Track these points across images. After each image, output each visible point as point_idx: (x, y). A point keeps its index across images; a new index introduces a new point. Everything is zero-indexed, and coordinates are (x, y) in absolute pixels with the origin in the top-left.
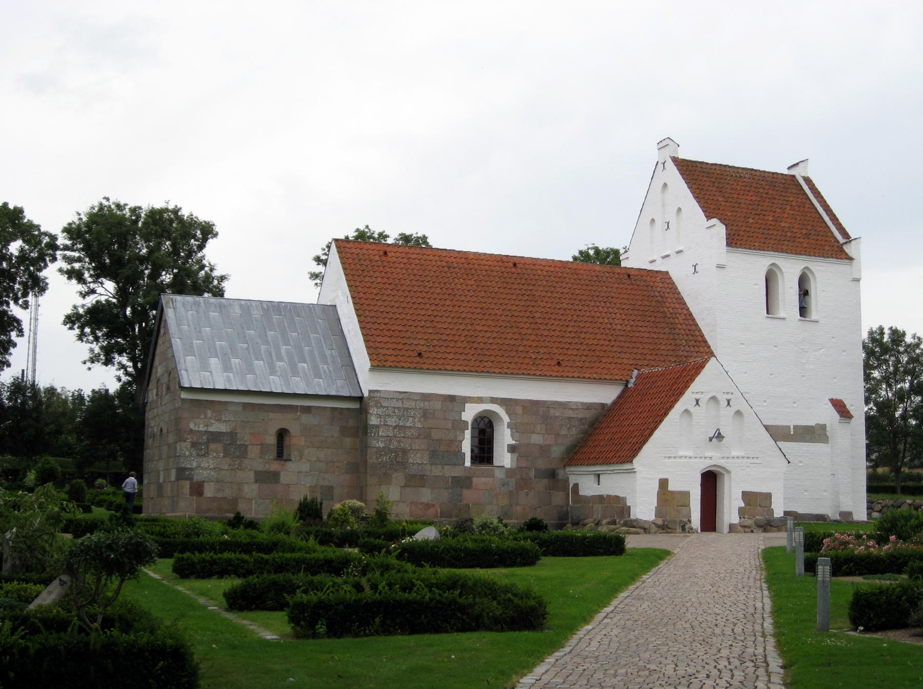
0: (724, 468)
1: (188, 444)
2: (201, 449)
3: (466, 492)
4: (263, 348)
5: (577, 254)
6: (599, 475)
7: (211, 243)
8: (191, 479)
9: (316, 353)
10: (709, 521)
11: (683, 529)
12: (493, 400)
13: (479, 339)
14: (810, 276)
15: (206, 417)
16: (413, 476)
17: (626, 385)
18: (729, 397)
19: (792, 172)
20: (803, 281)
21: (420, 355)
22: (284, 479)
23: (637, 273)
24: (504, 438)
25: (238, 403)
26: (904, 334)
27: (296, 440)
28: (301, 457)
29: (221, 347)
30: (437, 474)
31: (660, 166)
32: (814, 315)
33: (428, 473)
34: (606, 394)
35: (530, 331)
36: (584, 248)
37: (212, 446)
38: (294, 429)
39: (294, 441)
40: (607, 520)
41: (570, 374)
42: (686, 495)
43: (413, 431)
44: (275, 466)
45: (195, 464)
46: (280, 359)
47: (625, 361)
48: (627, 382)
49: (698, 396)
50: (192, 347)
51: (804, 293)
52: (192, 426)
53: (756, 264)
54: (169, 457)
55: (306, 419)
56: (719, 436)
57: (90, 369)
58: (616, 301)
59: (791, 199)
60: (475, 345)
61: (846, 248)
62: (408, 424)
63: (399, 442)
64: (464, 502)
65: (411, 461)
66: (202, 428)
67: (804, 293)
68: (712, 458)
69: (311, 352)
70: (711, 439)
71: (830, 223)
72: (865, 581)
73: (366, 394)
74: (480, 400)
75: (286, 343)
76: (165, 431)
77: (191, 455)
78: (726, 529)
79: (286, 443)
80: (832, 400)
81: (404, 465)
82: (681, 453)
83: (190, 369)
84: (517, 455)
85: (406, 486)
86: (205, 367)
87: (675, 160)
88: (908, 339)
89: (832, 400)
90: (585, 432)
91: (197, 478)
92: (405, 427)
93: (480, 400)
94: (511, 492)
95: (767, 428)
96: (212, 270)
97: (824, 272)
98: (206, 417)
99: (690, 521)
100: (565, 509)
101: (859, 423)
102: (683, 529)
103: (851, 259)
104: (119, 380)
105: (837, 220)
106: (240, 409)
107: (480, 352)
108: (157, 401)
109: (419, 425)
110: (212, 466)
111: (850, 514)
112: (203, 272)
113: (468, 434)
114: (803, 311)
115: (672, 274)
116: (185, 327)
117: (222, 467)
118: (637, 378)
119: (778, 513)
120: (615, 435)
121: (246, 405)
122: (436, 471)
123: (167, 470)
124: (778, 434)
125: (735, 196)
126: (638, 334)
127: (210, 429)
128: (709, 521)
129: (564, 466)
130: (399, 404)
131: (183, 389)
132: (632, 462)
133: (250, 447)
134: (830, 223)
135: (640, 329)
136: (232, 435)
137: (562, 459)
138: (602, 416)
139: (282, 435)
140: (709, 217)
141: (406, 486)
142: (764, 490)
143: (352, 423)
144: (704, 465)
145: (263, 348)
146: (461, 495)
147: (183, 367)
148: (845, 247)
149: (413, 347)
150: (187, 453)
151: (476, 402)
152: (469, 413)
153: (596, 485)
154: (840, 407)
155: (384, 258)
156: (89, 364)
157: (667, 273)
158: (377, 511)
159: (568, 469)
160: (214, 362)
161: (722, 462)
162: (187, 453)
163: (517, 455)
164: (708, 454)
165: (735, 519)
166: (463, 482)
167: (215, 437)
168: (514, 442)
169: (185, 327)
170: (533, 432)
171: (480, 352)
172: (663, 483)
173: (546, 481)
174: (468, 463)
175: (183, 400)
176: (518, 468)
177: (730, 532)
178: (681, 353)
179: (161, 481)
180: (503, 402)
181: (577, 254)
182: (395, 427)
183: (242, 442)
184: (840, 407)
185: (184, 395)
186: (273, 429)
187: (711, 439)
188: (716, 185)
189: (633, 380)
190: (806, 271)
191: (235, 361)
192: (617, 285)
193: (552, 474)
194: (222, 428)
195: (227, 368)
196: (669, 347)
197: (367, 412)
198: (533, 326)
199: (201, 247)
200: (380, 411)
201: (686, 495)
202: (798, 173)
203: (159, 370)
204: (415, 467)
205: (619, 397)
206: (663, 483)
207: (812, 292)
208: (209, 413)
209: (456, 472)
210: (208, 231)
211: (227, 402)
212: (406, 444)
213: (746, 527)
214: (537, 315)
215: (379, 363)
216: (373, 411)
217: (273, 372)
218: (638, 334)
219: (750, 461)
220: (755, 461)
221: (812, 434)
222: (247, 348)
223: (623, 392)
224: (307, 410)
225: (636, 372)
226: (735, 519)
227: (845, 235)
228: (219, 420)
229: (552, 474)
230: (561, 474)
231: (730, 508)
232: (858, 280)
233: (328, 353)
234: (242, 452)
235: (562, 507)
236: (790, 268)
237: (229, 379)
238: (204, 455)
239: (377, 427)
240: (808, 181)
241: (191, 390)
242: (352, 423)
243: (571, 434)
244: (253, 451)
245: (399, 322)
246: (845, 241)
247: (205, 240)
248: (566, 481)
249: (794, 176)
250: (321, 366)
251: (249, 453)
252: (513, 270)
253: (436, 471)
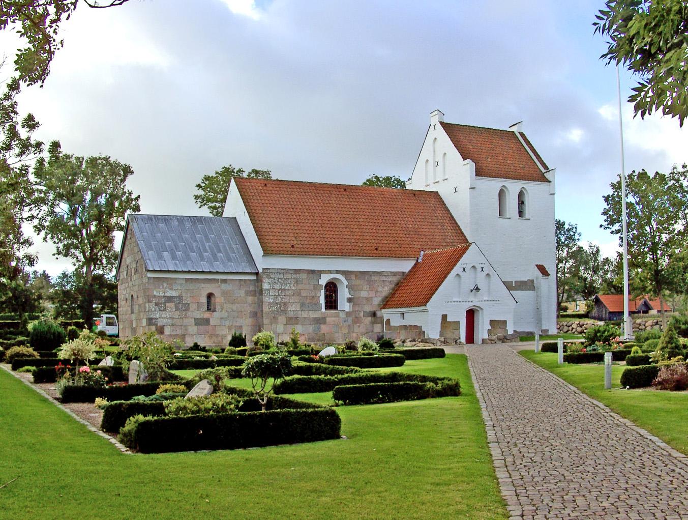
0: (479, 307)
1: (153, 304)
2: (161, 307)
3: (323, 326)
4: (207, 245)
5: (562, 221)
6: (403, 314)
7: (130, 177)
8: (156, 325)
9: (227, 247)
10: (470, 339)
11: (456, 342)
12: (338, 272)
13: (327, 236)
14: (505, 190)
15: (163, 287)
16: (291, 318)
17: (417, 261)
18: (482, 266)
19: (511, 129)
20: (521, 195)
21: (293, 246)
22: (212, 322)
23: (419, 193)
24: (343, 294)
25: (183, 279)
26: (564, 223)
27: (218, 299)
28: (222, 309)
29: (169, 245)
30: (306, 316)
31: (432, 127)
32: (527, 216)
33: (300, 316)
34: (406, 266)
35: (357, 230)
36: (369, 177)
37: (168, 305)
38: (217, 293)
39: (217, 300)
40: (410, 340)
41: (384, 255)
42: (458, 323)
43: (290, 292)
44: (207, 315)
45: (158, 316)
46: (206, 251)
47: (416, 246)
48: (418, 258)
49: (464, 266)
50: (151, 246)
51: (521, 203)
52: (155, 293)
53: (493, 185)
54: (139, 312)
55: (224, 287)
56: (477, 289)
57: (57, 258)
58: (408, 210)
59: (512, 146)
60: (326, 239)
61: (547, 175)
62: (287, 288)
63: (282, 298)
64: (322, 332)
65: (289, 309)
66: (161, 294)
67: (521, 203)
68: (473, 301)
69: (224, 247)
70: (472, 291)
71: (536, 160)
72: (445, 401)
73: (261, 271)
74: (330, 272)
75: (208, 240)
76: (135, 296)
77: (155, 310)
78: (480, 342)
79: (212, 301)
80: (537, 265)
81: (285, 312)
82: (455, 299)
83: (152, 259)
84: (352, 304)
85: (287, 324)
86: (160, 257)
87: (442, 123)
88: (566, 226)
89: (537, 265)
90: (393, 289)
91: (159, 324)
92: (284, 290)
93: (330, 272)
94: (349, 326)
95: (504, 283)
96: (130, 193)
97: (533, 189)
98: (163, 287)
99: (460, 338)
100: (381, 334)
101: (553, 278)
102: (456, 342)
103: (550, 182)
104: (75, 265)
105: (541, 158)
106: (237, 283)
107: (328, 243)
108: (127, 279)
109: (294, 288)
110: (168, 317)
111: (547, 331)
112: (125, 197)
113: (323, 292)
114: (521, 214)
115: (439, 193)
116: (145, 234)
117: (175, 317)
118: (424, 256)
119: (510, 332)
120: (412, 291)
121: (187, 280)
122: (305, 314)
123: (139, 320)
124: (509, 286)
125: (479, 145)
126: (422, 230)
127: (166, 295)
128: (470, 339)
129: (381, 309)
130: (281, 276)
131: (149, 271)
132: (426, 305)
133: (190, 305)
134: (536, 160)
135: (423, 227)
136: (180, 297)
137: (379, 305)
138: (406, 277)
139: (210, 296)
140: (464, 159)
141: (287, 324)
142: (502, 319)
143: (252, 288)
144: (468, 306)
145: (207, 245)
146: (320, 328)
147: (147, 258)
148: (545, 174)
149: (288, 242)
150: (153, 309)
151: (327, 273)
152: (324, 280)
153: (402, 320)
154: (542, 270)
155: (265, 188)
156: (56, 256)
157: (437, 192)
158: (292, 339)
159: (383, 310)
160: (165, 254)
161: (478, 304)
162: (153, 309)
163: (352, 304)
164: (470, 299)
165: (486, 336)
166: (320, 321)
167: (170, 299)
168: (350, 296)
169: (145, 234)
170: (362, 290)
171: (328, 243)
172: (444, 317)
173: (370, 319)
174: (323, 309)
175: (149, 278)
176: (353, 311)
177: (483, 343)
178: (449, 241)
179: (134, 326)
180: (343, 273)
181: (562, 221)
182: (279, 290)
183: (186, 302)
184: (542, 270)
185: (150, 275)
186: (204, 294)
187: (472, 291)
188: (467, 138)
189: (421, 258)
190: (523, 190)
191: (179, 254)
192: (407, 201)
193: (374, 314)
194: (174, 294)
195: (174, 257)
196: (441, 237)
197: (262, 281)
198: (359, 227)
199: (123, 180)
200: (270, 281)
201: (458, 323)
202: (514, 129)
203: (127, 260)
204: (292, 313)
205: (413, 268)
206: (444, 317)
207: (526, 202)
208: (165, 285)
209: (317, 315)
210: (127, 171)
211: (176, 278)
212: (286, 300)
213: (491, 340)
214: (361, 220)
215: (267, 252)
216: (266, 280)
217: (202, 259)
218: (422, 230)
219: (495, 302)
220: (497, 302)
221: (528, 285)
222: (185, 245)
223: (415, 265)
224: (224, 281)
225: (422, 252)
226: (486, 336)
227: (546, 167)
228: (171, 289)
229: (374, 314)
230: (379, 314)
231: (482, 330)
232: (554, 194)
233: (234, 246)
234: (187, 307)
235: (379, 333)
236: (513, 187)
237: (176, 264)
238: (163, 310)
239: (268, 290)
240: (522, 135)
241: (154, 271)
242: (252, 288)
243: (386, 290)
244: (193, 307)
245: (278, 227)
246: (546, 171)
247: (125, 176)
248: (382, 318)
249: (514, 132)
250: (231, 255)
251: (191, 308)
252: (345, 193)
253: (305, 314)
